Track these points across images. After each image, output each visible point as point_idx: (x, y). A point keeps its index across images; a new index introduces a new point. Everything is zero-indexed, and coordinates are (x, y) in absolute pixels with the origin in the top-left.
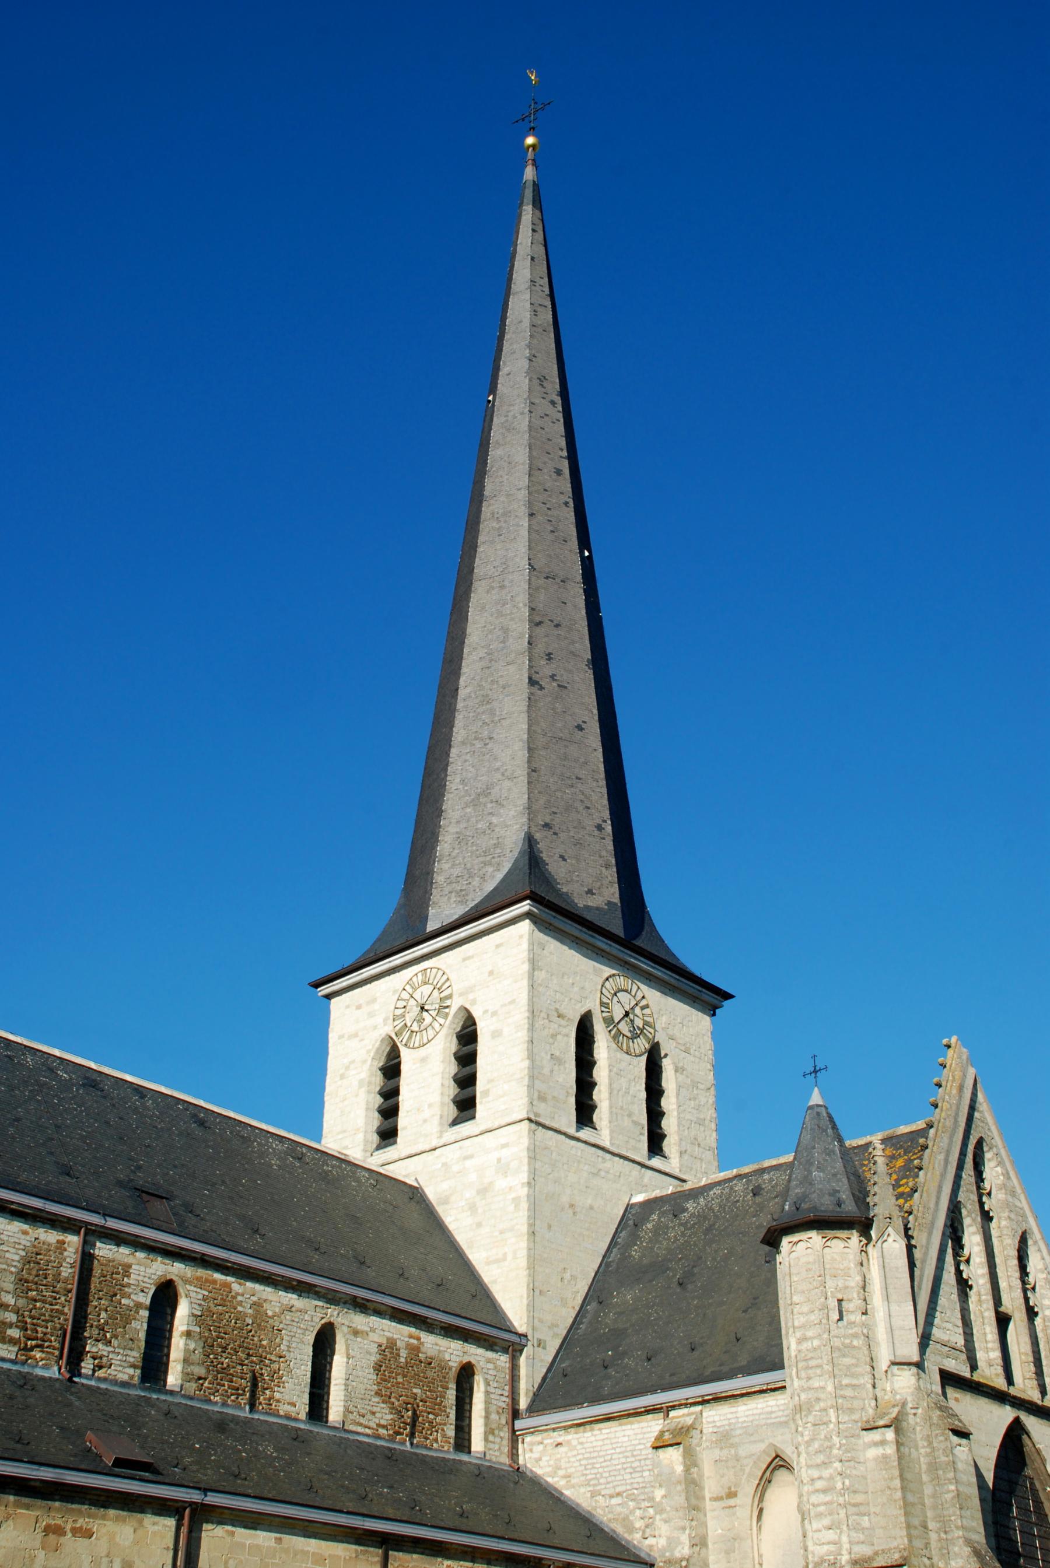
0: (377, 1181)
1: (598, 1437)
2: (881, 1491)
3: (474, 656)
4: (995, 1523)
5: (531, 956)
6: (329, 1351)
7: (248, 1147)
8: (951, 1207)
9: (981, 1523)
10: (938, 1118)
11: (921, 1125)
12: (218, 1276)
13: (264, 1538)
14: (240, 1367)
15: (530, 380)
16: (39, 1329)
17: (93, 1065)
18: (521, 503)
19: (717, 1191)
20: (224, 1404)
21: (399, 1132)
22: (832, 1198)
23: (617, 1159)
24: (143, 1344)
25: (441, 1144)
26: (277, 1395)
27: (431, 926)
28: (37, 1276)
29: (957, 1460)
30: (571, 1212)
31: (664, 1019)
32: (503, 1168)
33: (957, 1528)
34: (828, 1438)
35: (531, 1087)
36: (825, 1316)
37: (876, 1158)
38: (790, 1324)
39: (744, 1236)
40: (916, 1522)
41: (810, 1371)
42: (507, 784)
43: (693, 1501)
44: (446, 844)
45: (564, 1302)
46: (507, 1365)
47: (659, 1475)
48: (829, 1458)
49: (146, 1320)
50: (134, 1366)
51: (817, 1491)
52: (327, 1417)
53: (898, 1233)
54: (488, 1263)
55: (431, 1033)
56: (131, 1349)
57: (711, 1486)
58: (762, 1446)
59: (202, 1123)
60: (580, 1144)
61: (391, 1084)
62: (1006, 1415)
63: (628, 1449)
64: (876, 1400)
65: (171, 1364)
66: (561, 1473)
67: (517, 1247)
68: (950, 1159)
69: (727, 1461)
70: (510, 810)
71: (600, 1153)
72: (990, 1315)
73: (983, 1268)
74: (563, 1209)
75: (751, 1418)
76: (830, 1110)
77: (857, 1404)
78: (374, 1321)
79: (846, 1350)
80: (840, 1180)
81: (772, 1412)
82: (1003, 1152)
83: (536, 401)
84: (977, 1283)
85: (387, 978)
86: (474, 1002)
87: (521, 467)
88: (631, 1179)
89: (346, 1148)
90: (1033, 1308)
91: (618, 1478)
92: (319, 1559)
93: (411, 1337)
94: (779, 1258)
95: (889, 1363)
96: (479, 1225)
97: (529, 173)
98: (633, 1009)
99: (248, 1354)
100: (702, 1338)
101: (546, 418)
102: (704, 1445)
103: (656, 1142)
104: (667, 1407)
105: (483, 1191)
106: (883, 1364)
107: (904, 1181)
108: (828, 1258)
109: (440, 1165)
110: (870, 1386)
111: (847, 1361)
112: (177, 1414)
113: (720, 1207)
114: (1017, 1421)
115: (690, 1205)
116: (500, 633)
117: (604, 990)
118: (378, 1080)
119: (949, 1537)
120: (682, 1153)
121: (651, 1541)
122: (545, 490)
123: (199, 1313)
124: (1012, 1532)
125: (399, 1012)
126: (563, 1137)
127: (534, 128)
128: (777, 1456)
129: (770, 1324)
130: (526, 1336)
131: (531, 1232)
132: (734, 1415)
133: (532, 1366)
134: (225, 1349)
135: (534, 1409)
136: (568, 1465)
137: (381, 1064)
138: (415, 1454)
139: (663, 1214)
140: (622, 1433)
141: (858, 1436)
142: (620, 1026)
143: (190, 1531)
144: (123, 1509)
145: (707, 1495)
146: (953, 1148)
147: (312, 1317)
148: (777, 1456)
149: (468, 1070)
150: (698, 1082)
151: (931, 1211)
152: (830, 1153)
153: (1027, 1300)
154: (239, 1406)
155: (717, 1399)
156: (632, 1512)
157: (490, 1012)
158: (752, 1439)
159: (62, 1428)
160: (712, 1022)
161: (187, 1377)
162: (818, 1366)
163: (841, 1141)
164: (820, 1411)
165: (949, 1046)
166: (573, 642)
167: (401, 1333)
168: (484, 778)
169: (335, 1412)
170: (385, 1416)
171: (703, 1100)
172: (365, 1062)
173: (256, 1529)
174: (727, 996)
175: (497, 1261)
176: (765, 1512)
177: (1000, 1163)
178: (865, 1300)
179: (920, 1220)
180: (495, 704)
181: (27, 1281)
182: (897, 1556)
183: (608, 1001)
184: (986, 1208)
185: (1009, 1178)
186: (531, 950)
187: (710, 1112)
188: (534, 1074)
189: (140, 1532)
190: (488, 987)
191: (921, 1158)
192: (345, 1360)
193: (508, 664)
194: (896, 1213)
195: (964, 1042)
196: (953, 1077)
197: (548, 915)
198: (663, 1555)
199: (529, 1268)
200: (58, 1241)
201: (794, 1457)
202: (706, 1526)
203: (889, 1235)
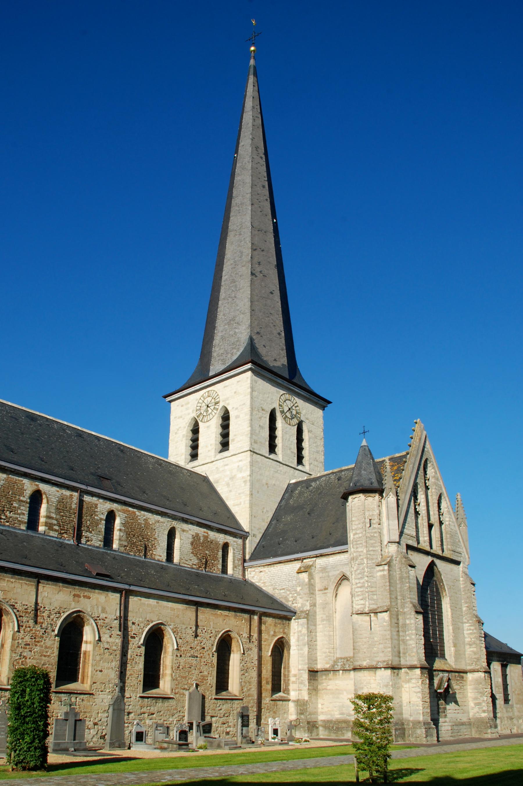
0: (190, 474)
3: (229, 263)
4: (422, 596)
6: (173, 537)
7: (140, 460)
9: (417, 596)
11: (404, 453)
12: (130, 509)
13: (152, 602)
14: (140, 542)
15: (252, 148)
16: (65, 527)
17: (79, 428)
18: (248, 199)
19: (324, 478)
20: (135, 555)
21: (199, 455)
23: (285, 466)
24: (103, 533)
25: (215, 460)
26: (154, 553)
27: (211, 374)
28: (63, 507)
30: (266, 486)
32: (240, 469)
33: (408, 598)
34: (363, 569)
35: (251, 438)
38: (351, 528)
39: (334, 496)
40: (393, 597)
42: (242, 316)
43: (312, 591)
44: (217, 341)
45: (263, 520)
46: (242, 543)
47: (299, 582)
49: (104, 524)
50: (100, 541)
51: (358, 587)
52: (173, 561)
54: (234, 506)
55: (211, 416)
56: (99, 535)
57: (318, 585)
58: (338, 572)
59: (122, 451)
60: (270, 460)
61: (196, 436)
65: (114, 541)
66: (262, 581)
67: (245, 500)
70: (243, 327)
71: (278, 464)
72: (426, 524)
75: (334, 562)
77: (374, 557)
78: (190, 526)
80: (372, 475)
81: (342, 560)
82: (435, 464)
83: (255, 157)
85: (194, 394)
86: (228, 404)
87: (248, 184)
89: (178, 461)
90: (442, 521)
92: (173, 609)
93: (204, 532)
94: (347, 504)
96: (231, 491)
97: (252, 62)
98: (292, 407)
99: (143, 538)
101: (258, 164)
102: (316, 572)
103: (300, 459)
105: (232, 478)
106: (385, 542)
107: (397, 475)
108: (366, 504)
109: (215, 468)
110: (380, 550)
112: (117, 558)
114: (433, 561)
115: (313, 484)
116: (239, 253)
118: (190, 435)
119: (405, 601)
120: (310, 464)
121: (295, 605)
122: (258, 194)
123: (124, 523)
124: (427, 599)
125: (198, 408)
126: (264, 457)
127: (254, 44)
128: (344, 575)
129: (343, 528)
130: (248, 533)
133: (251, 543)
134: (134, 536)
135: (251, 559)
137: (191, 428)
138: (207, 574)
139: (302, 487)
141: (374, 568)
142: (287, 414)
143: (125, 598)
144: (101, 590)
145: (317, 589)
147: (167, 525)
148: (344, 575)
149: (226, 431)
152: (369, 464)
153: (440, 518)
154: (140, 556)
155: (322, 555)
156: (288, 595)
158: (335, 569)
159: (76, 562)
160: (323, 413)
161: (120, 545)
162: (361, 544)
163: (373, 459)
166: (269, 257)
167: (201, 531)
168: (233, 313)
169: (176, 558)
170: (196, 561)
171: (319, 444)
172: (185, 427)
173: (149, 598)
174: (329, 402)
175: (237, 505)
176: (338, 595)
177: (433, 468)
178: (380, 519)
179: (402, 490)
180: (237, 283)
181: (59, 509)
184: (427, 485)
185: (436, 474)
186: (251, 383)
188: (252, 433)
189: (107, 598)
191: (403, 466)
192: (180, 540)
193: (243, 266)
194: (393, 487)
195: (422, 421)
196: (418, 435)
197: (259, 369)
199: (250, 507)
200: (70, 495)
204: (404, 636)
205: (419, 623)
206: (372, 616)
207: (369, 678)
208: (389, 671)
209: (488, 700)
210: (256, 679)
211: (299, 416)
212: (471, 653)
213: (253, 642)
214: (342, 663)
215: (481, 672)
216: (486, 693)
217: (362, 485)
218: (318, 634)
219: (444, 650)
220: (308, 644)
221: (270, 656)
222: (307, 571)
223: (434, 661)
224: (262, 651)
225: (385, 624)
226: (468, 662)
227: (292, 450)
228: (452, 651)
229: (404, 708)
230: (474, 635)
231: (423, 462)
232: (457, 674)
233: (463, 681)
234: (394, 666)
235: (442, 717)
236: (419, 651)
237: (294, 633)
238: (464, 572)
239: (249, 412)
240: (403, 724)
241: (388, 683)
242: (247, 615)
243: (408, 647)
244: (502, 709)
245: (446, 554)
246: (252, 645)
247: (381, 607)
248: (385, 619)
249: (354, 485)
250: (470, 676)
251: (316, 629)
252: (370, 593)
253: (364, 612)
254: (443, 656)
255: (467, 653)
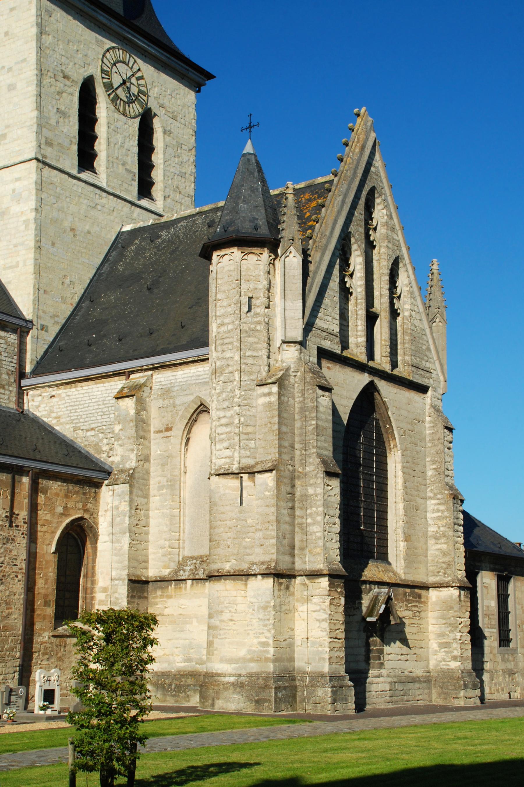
1: (80, 392)
2: (265, 425)
5: (39, 21)
8: (343, 236)
9: (331, 444)
10: (342, 169)
19: (183, 223)
22: (252, 224)
29: (320, 405)
30: (71, 234)
31: (156, 90)
32: (17, 197)
33: (313, 447)
34: (232, 391)
35: (39, 133)
36: (238, 308)
37: (287, 195)
40: (286, 444)
41: (224, 347)
43: (141, 433)
46: (16, 342)
48: (232, 404)
51: (222, 425)
53: (297, 251)
58: (192, 398)
62: (365, 379)
63: (101, 400)
64: (269, 366)
66: (53, 415)
68: (347, 200)
69: (167, 408)
71: (98, 191)
72: (362, 313)
73: (361, 280)
74: (65, 232)
75: (185, 379)
76: (259, 159)
79: (251, 332)
81: (200, 375)
82: (389, 199)
84: (356, 291)
88: (122, 213)
91: (93, 419)
94: (211, 268)
95: (281, 342)
98: (129, 78)
100: (159, 326)
102: (153, 397)
104: (129, 372)
108: (244, 267)
110: (265, 357)
111: (251, 340)
113: (184, 235)
114: (371, 383)
115: (163, 234)
117: (105, 60)
119: (307, 453)
124: (357, 452)
126: (67, 176)
128: (202, 404)
130: (31, 322)
131: (37, 246)
132: (174, 377)
136: (58, 410)
140: (97, 389)
145: (152, 429)
146: (350, 193)
148: (202, 404)
150: (182, 144)
151: (326, 237)
152: (254, 190)
155: (163, 366)
156: (101, 440)
157: (6, 68)
158: (185, 393)
160: (196, 97)
164: (228, 373)
165: (358, 115)
171: (185, 158)
174: (210, 76)
175: (11, 267)
176: (191, 440)
177: (386, 207)
178: (269, 298)
179: (317, 244)
182: (270, 464)
183: (108, 69)
186: (39, 15)
187: (190, 168)
190: (4, 46)
194: (298, 236)
196: (358, 139)
198: (118, 467)
201: (210, 403)
202: (150, 449)
203: (290, 252)
204: (302, 517)
205: (332, 493)
206: (243, 478)
207: (234, 593)
208: (270, 581)
209: (463, 639)
210: (22, 596)
211: (145, 98)
212: (437, 553)
213: (17, 526)
214: (192, 567)
215: (452, 587)
216: (461, 626)
217: (238, 231)
218: (151, 513)
219: (387, 547)
220: (130, 531)
221: (53, 553)
222: (133, 396)
223: (366, 565)
224: (36, 544)
225: (267, 493)
226: (431, 568)
227: (128, 167)
228: (401, 549)
229: (296, 649)
230: (445, 521)
231: (364, 193)
232: (408, 590)
233: (419, 602)
234: (281, 572)
235: (373, 668)
236: (328, 545)
237: (106, 511)
238: (434, 407)
239: (35, 77)
240: (293, 679)
241: (268, 602)
242: (5, 474)
243: (309, 537)
244: (495, 655)
245: (400, 372)
246: (16, 533)
247: (262, 462)
248: (268, 485)
249: (223, 230)
250: (433, 595)
251: (147, 503)
252: (243, 437)
253: (230, 471)
254: (383, 557)
255: (430, 552)
